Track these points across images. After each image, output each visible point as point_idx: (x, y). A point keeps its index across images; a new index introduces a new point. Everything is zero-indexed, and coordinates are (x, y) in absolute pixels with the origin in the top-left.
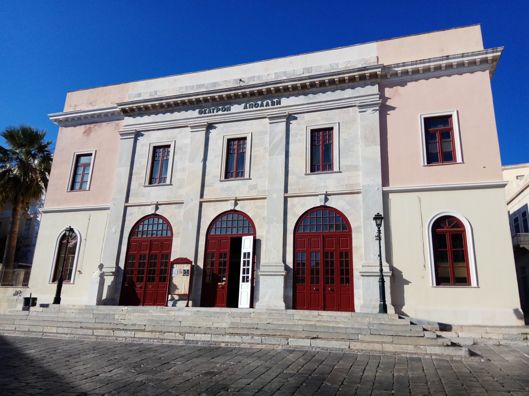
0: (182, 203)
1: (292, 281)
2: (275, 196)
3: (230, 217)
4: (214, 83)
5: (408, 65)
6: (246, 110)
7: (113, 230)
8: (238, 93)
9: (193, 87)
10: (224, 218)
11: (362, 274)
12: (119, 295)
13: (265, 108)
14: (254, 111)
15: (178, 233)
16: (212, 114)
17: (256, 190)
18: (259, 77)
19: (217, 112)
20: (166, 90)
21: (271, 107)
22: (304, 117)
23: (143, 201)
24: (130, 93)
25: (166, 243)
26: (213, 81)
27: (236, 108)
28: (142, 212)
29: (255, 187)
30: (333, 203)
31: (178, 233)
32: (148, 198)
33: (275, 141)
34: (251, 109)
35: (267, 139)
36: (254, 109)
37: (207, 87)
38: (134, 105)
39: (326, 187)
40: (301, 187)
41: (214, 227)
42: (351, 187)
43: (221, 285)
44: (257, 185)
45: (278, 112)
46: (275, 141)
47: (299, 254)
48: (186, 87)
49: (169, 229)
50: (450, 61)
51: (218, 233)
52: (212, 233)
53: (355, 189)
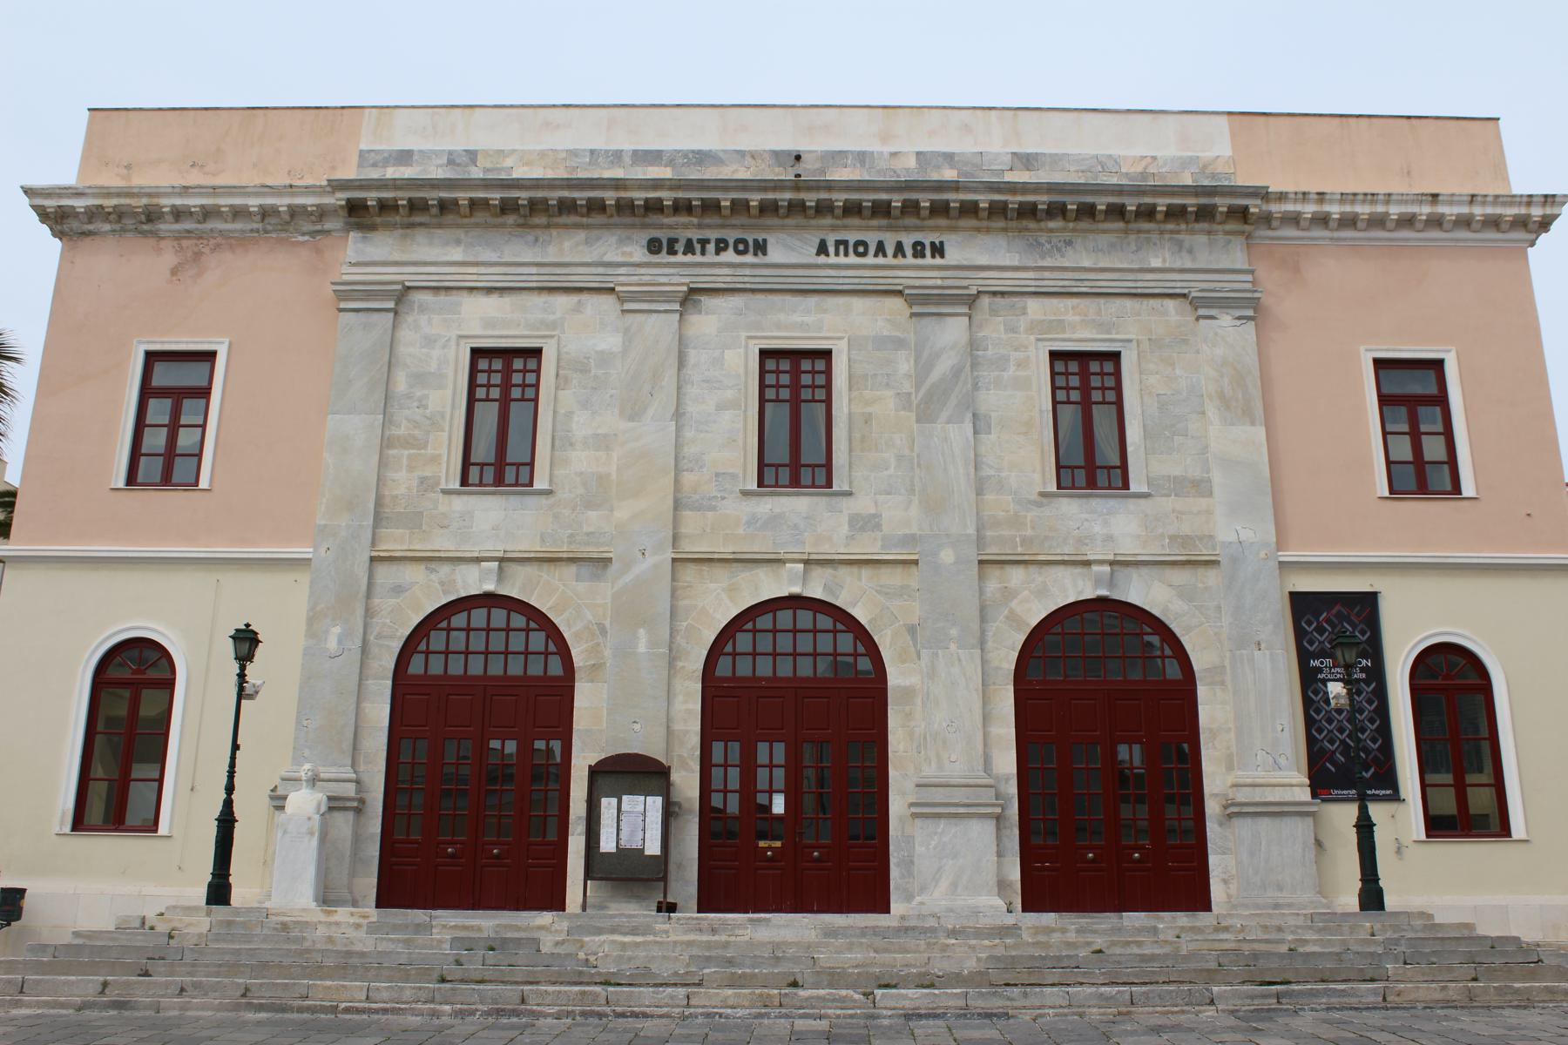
0: (606, 562)
1: (1017, 832)
2: (947, 556)
3: (479, 617)
4: (699, 152)
5: (248, 195)
6: (822, 259)
7: (332, 644)
8: (247, 206)
9: (617, 156)
10: (459, 620)
11: (914, 810)
12: (373, 881)
13: (890, 260)
14: (867, 268)
15: (596, 668)
16: (698, 258)
17: (879, 534)
18: (862, 157)
19: (718, 251)
20: (514, 151)
21: (910, 260)
22: (1025, 308)
23: (443, 543)
24: (363, 147)
25: (549, 701)
26: (696, 147)
27: (789, 249)
28: (442, 583)
29: (864, 524)
30: (1139, 592)
31: (596, 668)
32: (483, 540)
33: (935, 376)
34: (842, 260)
35: (904, 364)
36: (853, 259)
37: (671, 163)
38: (399, 194)
39: (1109, 538)
40: (1029, 532)
41: (422, 647)
42: (854, 543)
43: (770, 848)
44: (877, 516)
45: (939, 282)
46: (935, 376)
47: (406, 745)
48: (592, 152)
49: (552, 648)
50: (802, 195)
51: (436, 667)
52: (416, 666)
53: (1204, 552)
